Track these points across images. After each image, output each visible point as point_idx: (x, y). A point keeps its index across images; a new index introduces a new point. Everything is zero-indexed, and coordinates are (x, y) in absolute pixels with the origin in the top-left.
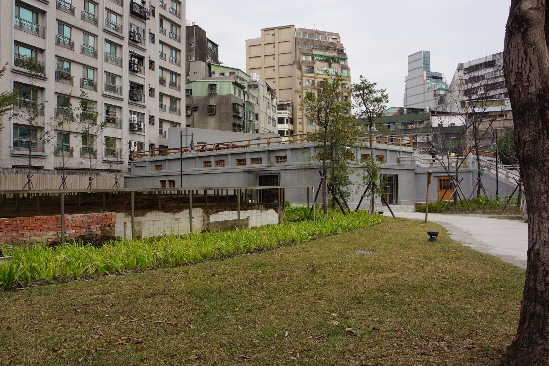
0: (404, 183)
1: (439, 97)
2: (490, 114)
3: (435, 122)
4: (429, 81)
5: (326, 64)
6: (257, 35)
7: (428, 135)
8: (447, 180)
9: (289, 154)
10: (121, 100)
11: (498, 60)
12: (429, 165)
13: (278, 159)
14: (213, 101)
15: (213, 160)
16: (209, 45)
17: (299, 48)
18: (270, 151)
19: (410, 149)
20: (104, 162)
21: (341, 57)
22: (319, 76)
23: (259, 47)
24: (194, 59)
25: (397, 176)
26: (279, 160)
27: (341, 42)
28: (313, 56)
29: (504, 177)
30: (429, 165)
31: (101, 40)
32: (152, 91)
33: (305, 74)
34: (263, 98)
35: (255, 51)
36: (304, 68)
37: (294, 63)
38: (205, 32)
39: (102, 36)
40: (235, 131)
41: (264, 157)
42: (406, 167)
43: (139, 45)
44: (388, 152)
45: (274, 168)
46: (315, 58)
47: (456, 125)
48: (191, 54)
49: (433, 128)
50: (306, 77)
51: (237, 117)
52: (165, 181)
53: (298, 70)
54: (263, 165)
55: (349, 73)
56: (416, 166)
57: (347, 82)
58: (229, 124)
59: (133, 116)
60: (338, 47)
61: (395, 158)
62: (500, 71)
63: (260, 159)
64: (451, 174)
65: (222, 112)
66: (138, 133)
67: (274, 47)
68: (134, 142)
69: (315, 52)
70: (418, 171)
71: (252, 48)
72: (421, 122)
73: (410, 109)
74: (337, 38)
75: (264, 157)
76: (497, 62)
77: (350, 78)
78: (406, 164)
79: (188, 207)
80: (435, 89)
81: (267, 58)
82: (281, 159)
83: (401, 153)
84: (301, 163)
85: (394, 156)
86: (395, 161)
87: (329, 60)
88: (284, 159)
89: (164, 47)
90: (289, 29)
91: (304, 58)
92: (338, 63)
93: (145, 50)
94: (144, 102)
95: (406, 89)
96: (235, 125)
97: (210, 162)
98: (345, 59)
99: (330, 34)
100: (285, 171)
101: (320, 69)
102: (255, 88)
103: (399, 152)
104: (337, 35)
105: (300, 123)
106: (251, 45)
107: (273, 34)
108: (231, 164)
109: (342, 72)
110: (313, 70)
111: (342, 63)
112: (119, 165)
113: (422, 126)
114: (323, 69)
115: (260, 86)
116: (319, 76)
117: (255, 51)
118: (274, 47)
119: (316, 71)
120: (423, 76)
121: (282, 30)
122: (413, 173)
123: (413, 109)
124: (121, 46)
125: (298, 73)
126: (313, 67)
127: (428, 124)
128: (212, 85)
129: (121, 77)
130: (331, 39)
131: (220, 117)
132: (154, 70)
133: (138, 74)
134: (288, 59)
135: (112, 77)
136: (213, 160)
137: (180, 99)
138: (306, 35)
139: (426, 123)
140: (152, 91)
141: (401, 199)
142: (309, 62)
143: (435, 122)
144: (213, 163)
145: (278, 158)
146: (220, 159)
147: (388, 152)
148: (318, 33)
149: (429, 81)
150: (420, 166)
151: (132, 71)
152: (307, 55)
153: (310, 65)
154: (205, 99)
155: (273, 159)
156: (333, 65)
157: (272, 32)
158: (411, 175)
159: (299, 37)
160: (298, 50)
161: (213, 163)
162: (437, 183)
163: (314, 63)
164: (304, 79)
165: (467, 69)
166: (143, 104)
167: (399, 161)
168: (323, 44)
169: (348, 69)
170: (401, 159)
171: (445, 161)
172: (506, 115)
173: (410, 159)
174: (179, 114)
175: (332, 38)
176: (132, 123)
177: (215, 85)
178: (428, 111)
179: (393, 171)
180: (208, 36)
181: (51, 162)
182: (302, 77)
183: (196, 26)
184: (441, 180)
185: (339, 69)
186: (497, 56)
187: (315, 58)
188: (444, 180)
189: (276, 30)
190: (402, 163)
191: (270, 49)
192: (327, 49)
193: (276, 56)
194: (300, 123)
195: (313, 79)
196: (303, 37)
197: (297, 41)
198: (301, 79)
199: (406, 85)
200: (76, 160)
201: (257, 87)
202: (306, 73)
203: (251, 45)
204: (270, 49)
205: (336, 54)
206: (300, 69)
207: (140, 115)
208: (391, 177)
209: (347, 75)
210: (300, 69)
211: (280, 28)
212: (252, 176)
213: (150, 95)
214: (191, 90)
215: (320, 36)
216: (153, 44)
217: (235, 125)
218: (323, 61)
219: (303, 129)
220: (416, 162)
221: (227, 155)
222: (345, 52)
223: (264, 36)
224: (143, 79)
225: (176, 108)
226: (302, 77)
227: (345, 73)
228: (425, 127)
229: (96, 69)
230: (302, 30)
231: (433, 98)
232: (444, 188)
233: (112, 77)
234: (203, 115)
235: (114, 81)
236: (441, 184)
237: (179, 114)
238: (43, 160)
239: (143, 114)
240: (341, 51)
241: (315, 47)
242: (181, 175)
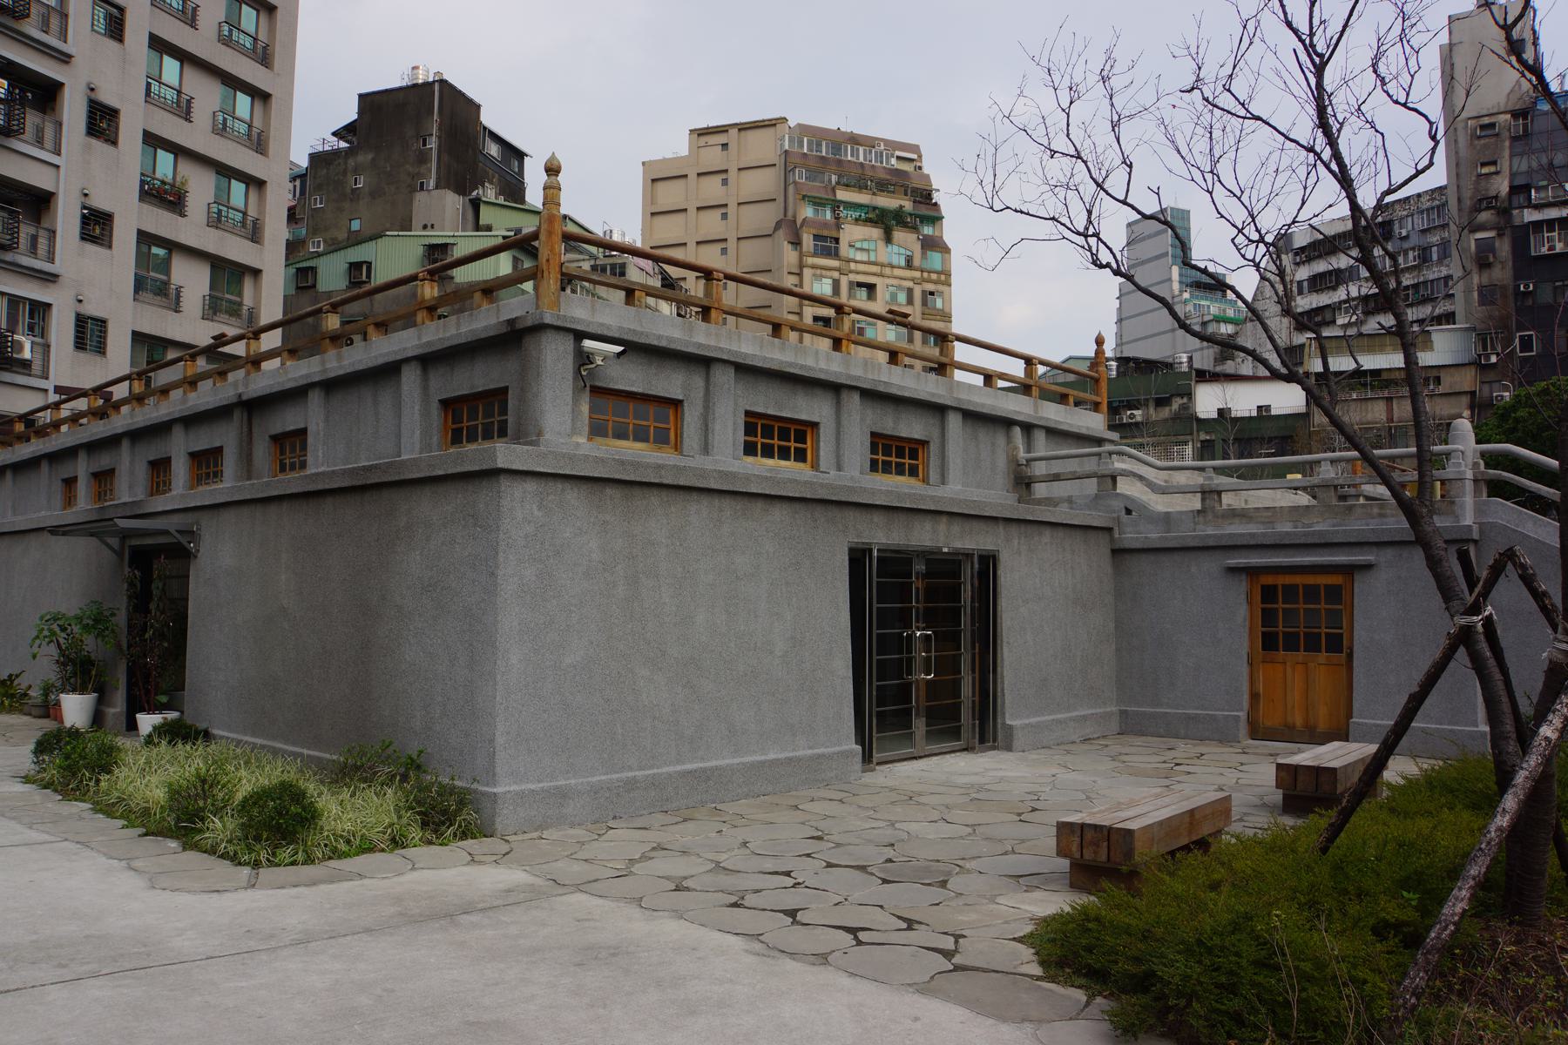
0: (1042, 610)
2: (1385, 376)
3: (1207, 401)
4: (1186, 295)
5: (876, 233)
6: (679, 146)
7: (1186, 443)
11: (1402, 218)
12: (1196, 503)
16: (493, 150)
17: (795, 182)
19: (1093, 422)
21: (924, 211)
22: (853, 266)
23: (681, 182)
24: (432, 183)
25: (988, 564)
27: (926, 170)
28: (836, 205)
30: (1196, 503)
33: (811, 260)
35: (671, 195)
36: (808, 241)
37: (778, 226)
38: (479, 107)
42: (1061, 514)
44: (954, 421)
46: (843, 213)
47: (1273, 412)
48: (423, 169)
49: (1199, 420)
50: (814, 267)
52: (1275, 587)
53: (787, 247)
55: (946, 262)
56: (1118, 505)
57: (941, 288)
60: (916, 183)
61: (1002, 461)
62: (1406, 253)
67: (725, 182)
69: (842, 195)
70: (1130, 536)
71: (660, 185)
72: (1161, 402)
73: (1127, 360)
74: (914, 156)
76: (1396, 226)
77: (948, 275)
78: (1067, 495)
80: (1206, 318)
81: (703, 213)
83: (1040, 437)
85: (996, 451)
86: (1002, 479)
87: (887, 222)
89: (188, 71)
90: (772, 130)
91: (808, 212)
92: (915, 229)
93: (65, 58)
94: (52, 260)
95: (1120, 321)
98: (936, 219)
99: (893, 145)
101: (858, 245)
103: (1028, 428)
104: (915, 149)
106: (658, 177)
107: (725, 146)
109: (924, 254)
110: (837, 249)
111: (927, 230)
113: (1165, 413)
114: (865, 245)
116: (853, 266)
117: (671, 195)
118: (725, 182)
119: (844, 249)
120: (1170, 279)
121: (751, 134)
122: (1102, 549)
123: (1136, 360)
125: (790, 256)
126: (837, 240)
127: (1184, 407)
130: (893, 161)
132: (114, 143)
134: (764, 217)
137: (256, 273)
138: (819, 145)
139: (1177, 403)
141: (1014, 715)
142: (825, 225)
143: (1207, 401)
147: (954, 421)
148: (855, 140)
149: (1186, 295)
150: (1143, 507)
152: (818, 203)
153: (825, 233)
156: (899, 235)
157: (722, 139)
158: (1085, 566)
159: (796, 149)
160: (791, 189)
162: (1242, 611)
163: (838, 227)
164: (807, 272)
165: (1303, 249)
166: (47, 267)
167: (1022, 482)
168: (869, 173)
169: (945, 250)
170: (1040, 469)
172: (1438, 380)
173: (1090, 465)
175: (899, 158)
177: (446, 245)
178: (1185, 368)
179: (956, 527)
180: (487, 118)
182: (801, 266)
183: (443, 82)
184: (1269, 593)
185: (917, 248)
186: (1397, 207)
187: (843, 213)
188: (1291, 592)
189: (734, 132)
190: (1040, 490)
191: (712, 190)
192: (882, 187)
193: (732, 210)
195: (836, 275)
196: (810, 149)
197: (789, 163)
198: (800, 275)
199: (1120, 309)
202: (815, 255)
203: (658, 177)
204: (712, 190)
205: (908, 205)
206: (796, 243)
208: (944, 567)
209: (938, 267)
210: (796, 243)
211: (743, 128)
214: (369, 264)
215: (861, 149)
218: (868, 221)
220: (1124, 486)
222: (936, 197)
223: (695, 149)
224: (52, 170)
225: (240, 304)
226: (801, 266)
227: (935, 259)
228: (1176, 418)
230: (804, 129)
236: (1268, 617)
240: (924, 196)
241: (845, 180)
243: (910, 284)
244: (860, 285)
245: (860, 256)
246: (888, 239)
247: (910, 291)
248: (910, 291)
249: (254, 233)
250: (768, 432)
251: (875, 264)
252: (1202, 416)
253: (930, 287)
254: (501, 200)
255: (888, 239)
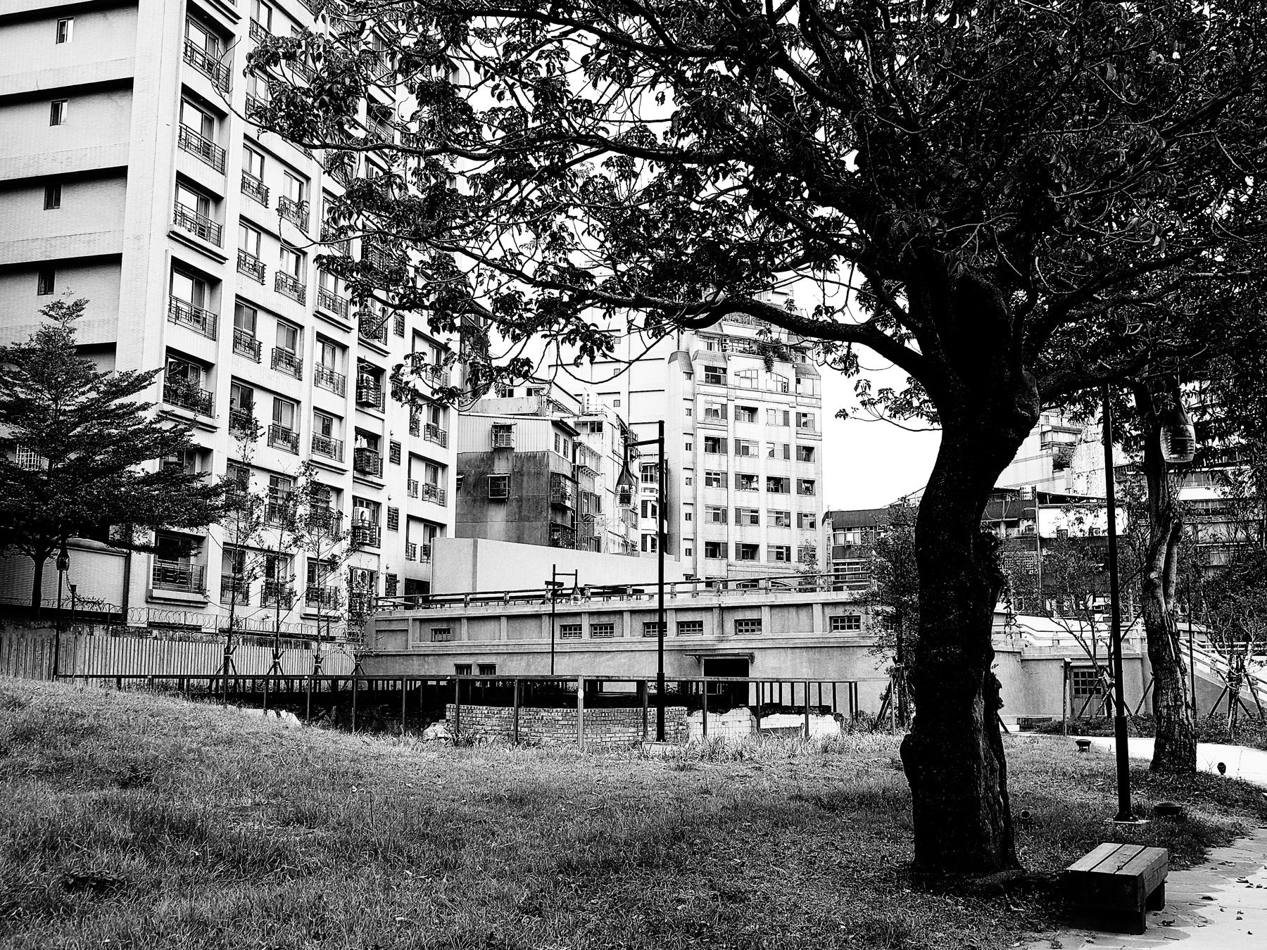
1: (1056, 449)
5: (759, 363)
8: (1090, 675)
9: (765, 615)
10: (341, 472)
13: (741, 625)
14: (502, 468)
15: (585, 623)
18: (723, 609)
20: (306, 617)
22: (739, 393)
26: (744, 628)
29: (1207, 670)
31: (308, 337)
32: (395, 448)
34: (611, 455)
39: (313, 326)
40: (555, 544)
41: (710, 621)
43: (376, 342)
45: (727, 645)
51: (560, 508)
54: (707, 637)
56: (1023, 644)
58: (541, 526)
59: (361, 509)
63: (700, 624)
64: (1099, 663)
65: (525, 494)
66: (367, 548)
68: (360, 572)
70: (1028, 654)
75: (710, 621)
79: (702, 707)
82: (747, 624)
84: (802, 635)
88: (753, 624)
96: (554, 527)
97: (580, 627)
100: (764, 652)
101: (742, 374)
102: (593, 430)
105: (688, 517)
108: (630, 632)
112: (269, 627)
113: (1014, 533)
115: (606, 427)
119: (731, 378)
124: (344, 348)
125: (686, 386)
126: (725, 370)
127: (1030, 529)
128: (502, 427)
129: (341, 418)
131: (520, 507)
133: (371, 411)
135: (327, 419)
136: (585, 623)
139: (1024, 525)
140: (395, 448)
144: (586, 629)
145: (738, 623)
146: (604, 620)
151: (362, 404)
153: (716, 364)
154: (482, 460)
155: (730, 626)
156: (778, 366)
160: (387, 90)
161: (586, 629)
166: (199, 597)
171: (1087, 635)
174: (443, 503)
176: (359, 528)
178: (1029, 497)
181: (214, 616)
188: (1083, 675)
194: (688, 517)
200: (255, 615)
201: (600, 430)
206: (690, 374)
207: (372, 507)
210: (690, 374)
212: (689, 660)
213: (392, 460)
216: (400, 339)
217: (554, 527)
219: (695, 534)
221: (621, 613)
229: (298, 402)
231: (1039, 453)
232: (1084, 691)
233: (327, 419)
234: (475, 501)
235: (327, 430)
237: (443, 503)
238: (200, 611)
239: (378, 505)
242: (553, 652)
243: (786, 408)
244: (744, 408)
245: (746, 384)
246: (769, 368)
247: (786, 413)
248: (786, 413)
249: (357, 501)
250: (836, 621)
251: (756, 390)
252: (1045, 536)
253: (803, 410)
254: (594, 149)
255: (769, 368)
